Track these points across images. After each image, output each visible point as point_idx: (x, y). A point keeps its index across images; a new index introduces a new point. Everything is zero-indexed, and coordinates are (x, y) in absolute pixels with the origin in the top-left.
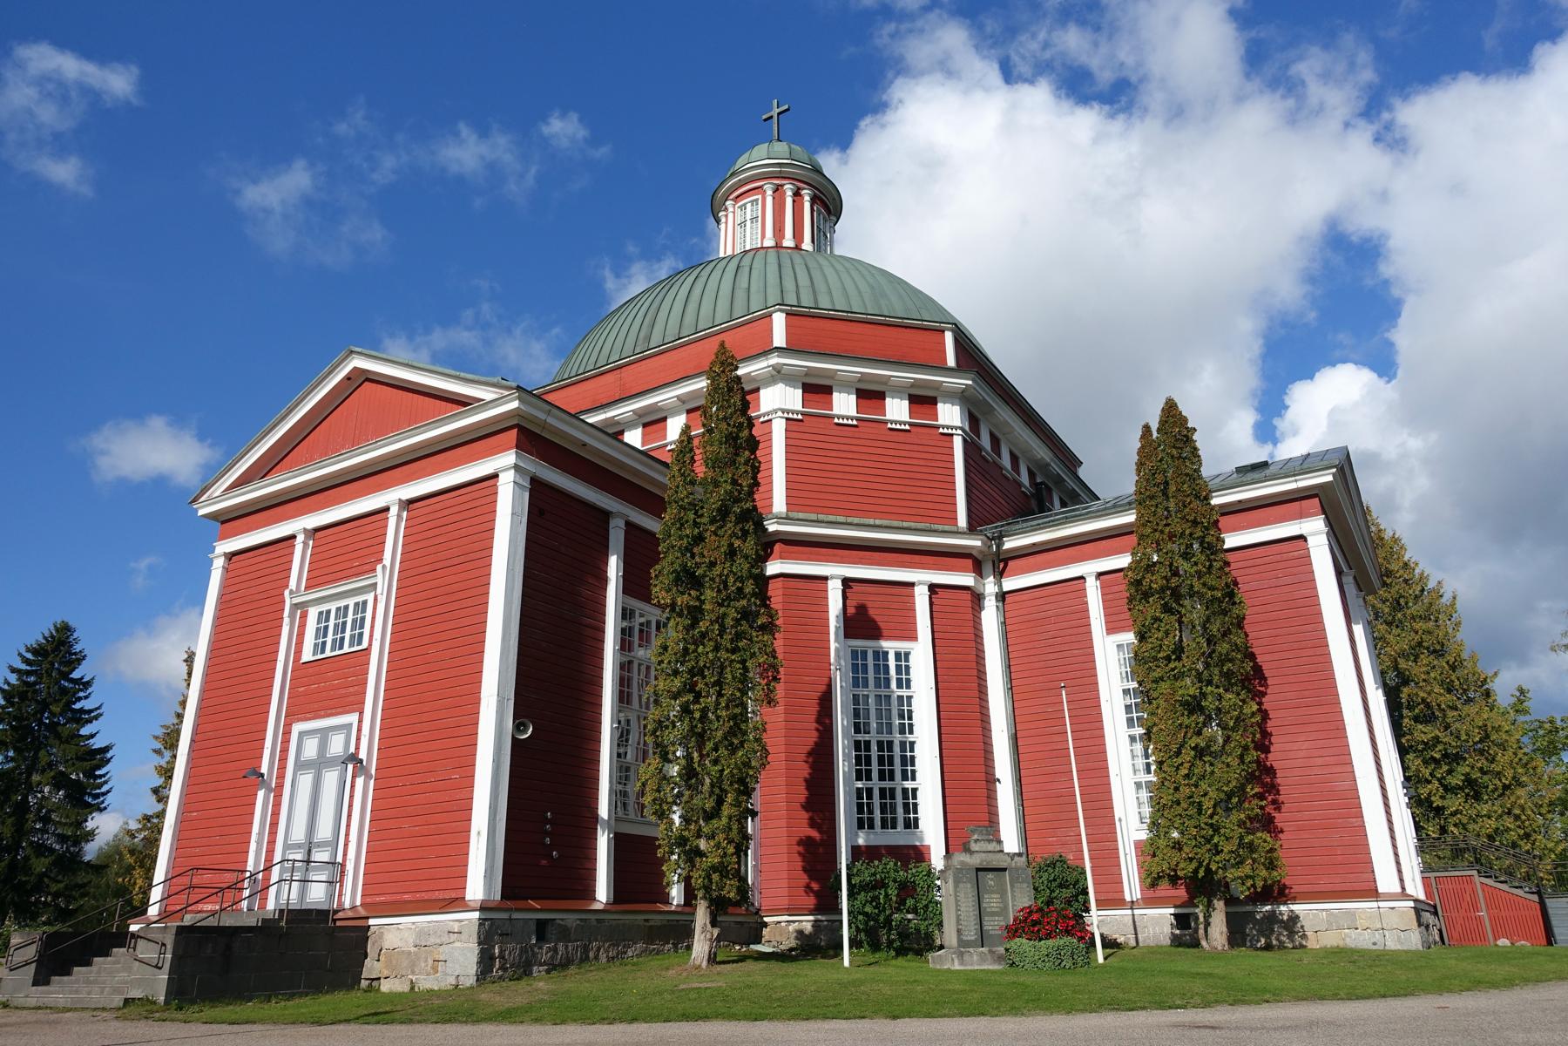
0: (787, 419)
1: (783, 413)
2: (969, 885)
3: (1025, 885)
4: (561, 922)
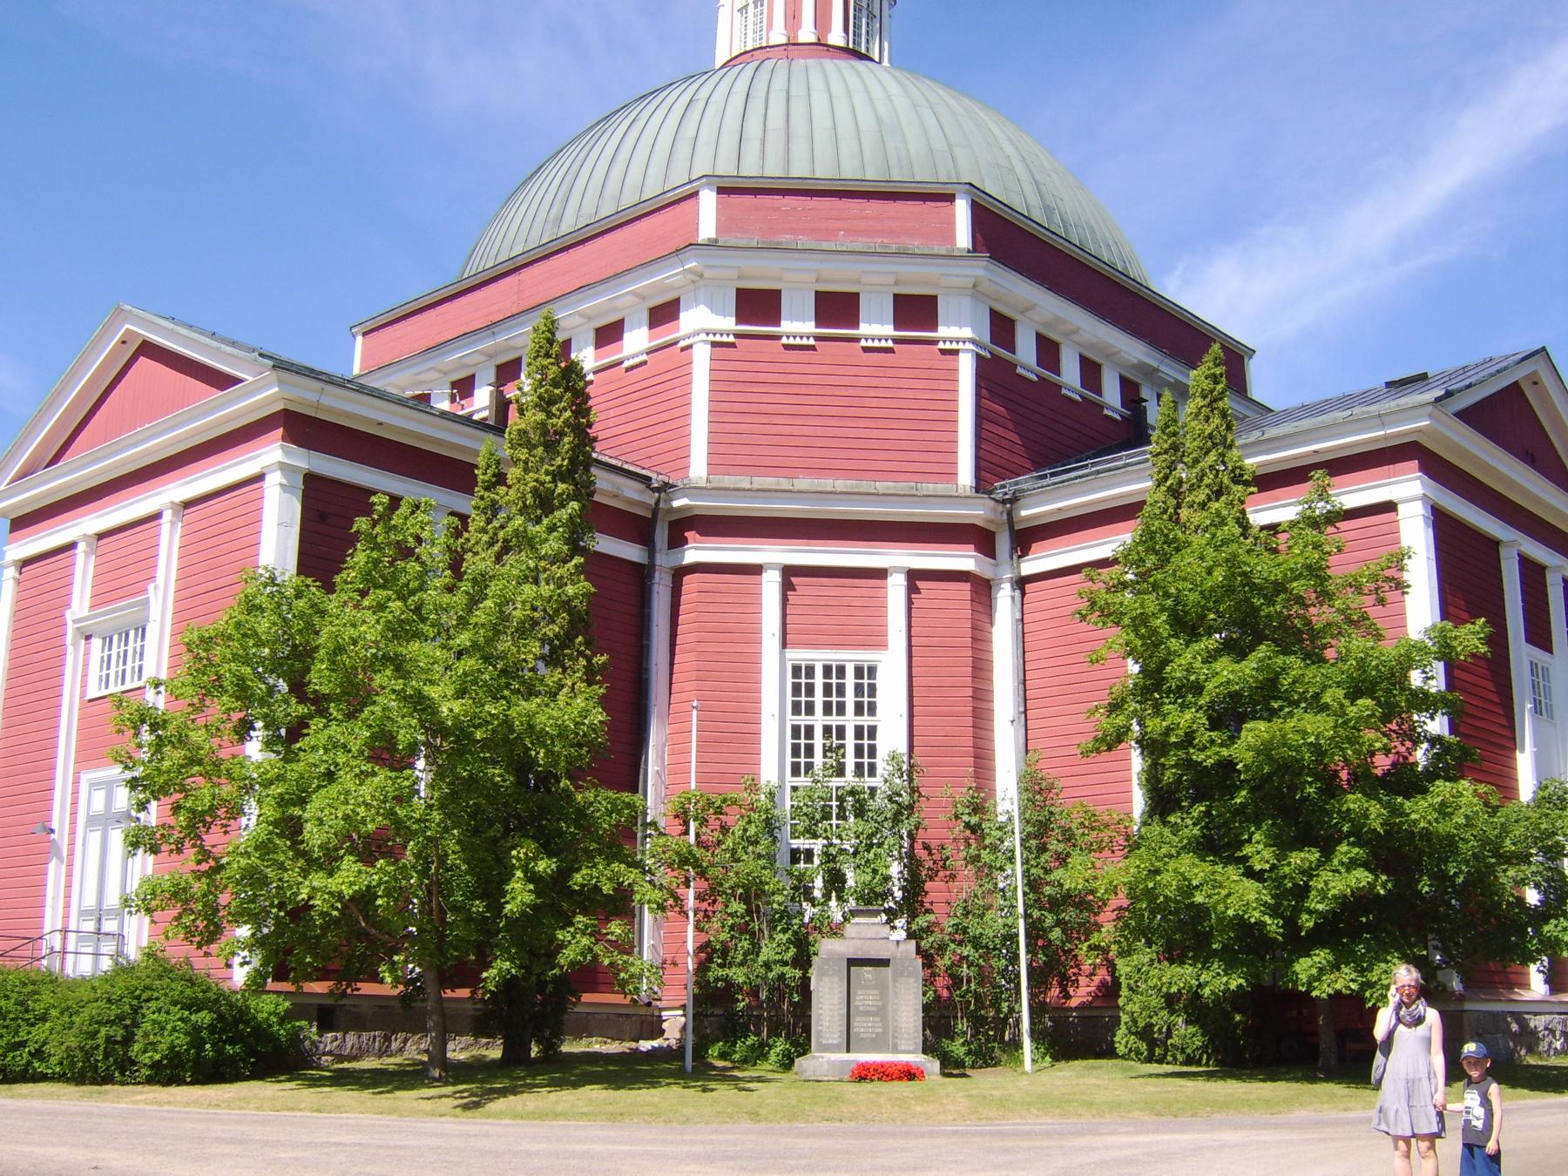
0: (714, 344)
1: (708, 334)
2: (836, 979)
3: (911, 980)
4: (352, 1009)
